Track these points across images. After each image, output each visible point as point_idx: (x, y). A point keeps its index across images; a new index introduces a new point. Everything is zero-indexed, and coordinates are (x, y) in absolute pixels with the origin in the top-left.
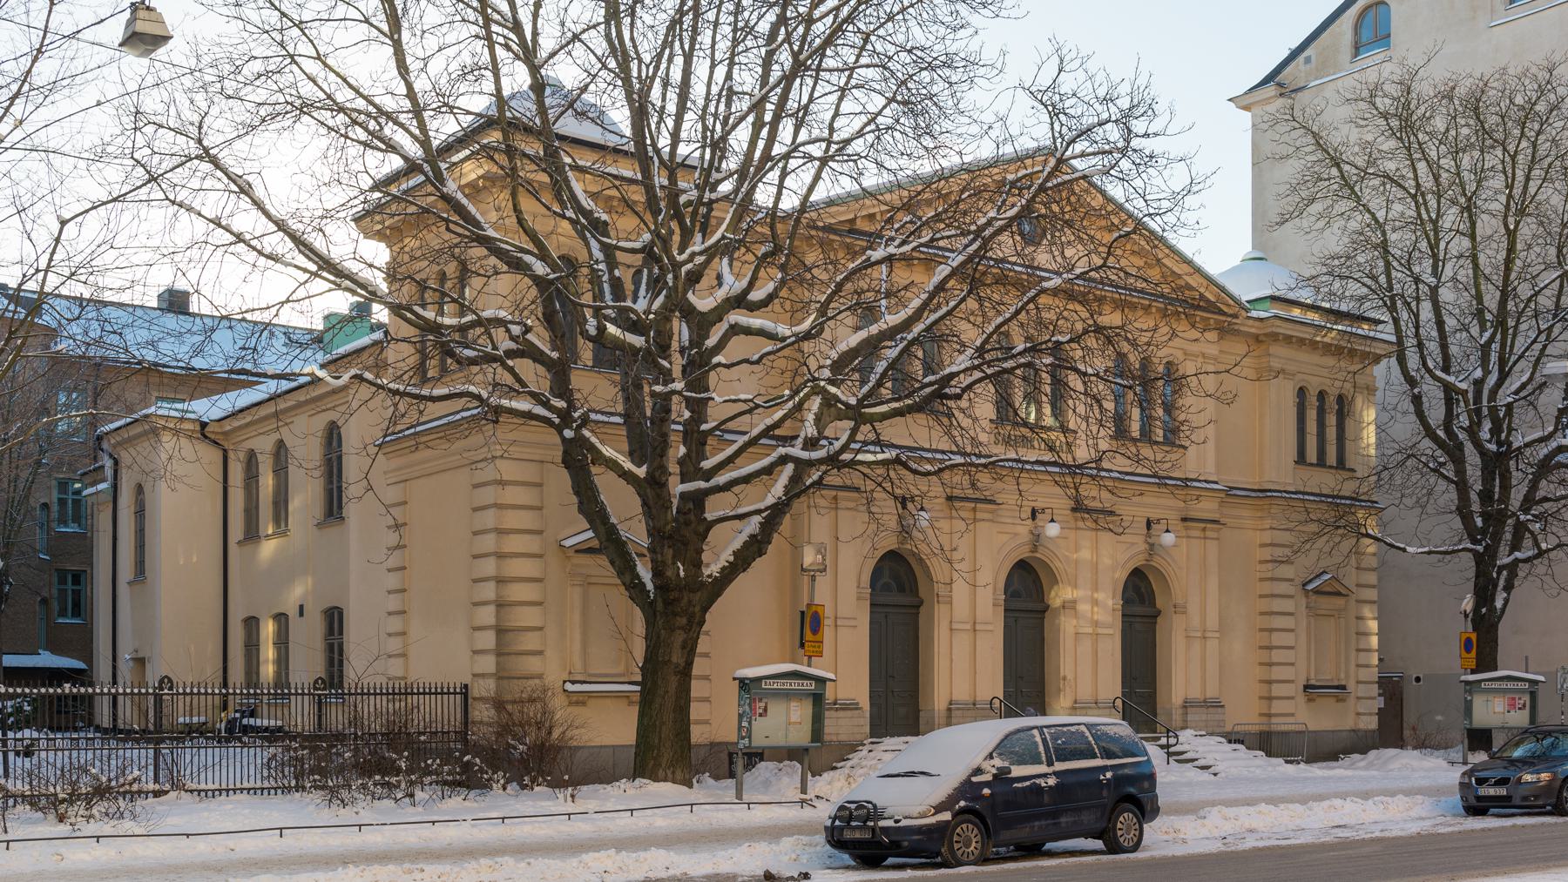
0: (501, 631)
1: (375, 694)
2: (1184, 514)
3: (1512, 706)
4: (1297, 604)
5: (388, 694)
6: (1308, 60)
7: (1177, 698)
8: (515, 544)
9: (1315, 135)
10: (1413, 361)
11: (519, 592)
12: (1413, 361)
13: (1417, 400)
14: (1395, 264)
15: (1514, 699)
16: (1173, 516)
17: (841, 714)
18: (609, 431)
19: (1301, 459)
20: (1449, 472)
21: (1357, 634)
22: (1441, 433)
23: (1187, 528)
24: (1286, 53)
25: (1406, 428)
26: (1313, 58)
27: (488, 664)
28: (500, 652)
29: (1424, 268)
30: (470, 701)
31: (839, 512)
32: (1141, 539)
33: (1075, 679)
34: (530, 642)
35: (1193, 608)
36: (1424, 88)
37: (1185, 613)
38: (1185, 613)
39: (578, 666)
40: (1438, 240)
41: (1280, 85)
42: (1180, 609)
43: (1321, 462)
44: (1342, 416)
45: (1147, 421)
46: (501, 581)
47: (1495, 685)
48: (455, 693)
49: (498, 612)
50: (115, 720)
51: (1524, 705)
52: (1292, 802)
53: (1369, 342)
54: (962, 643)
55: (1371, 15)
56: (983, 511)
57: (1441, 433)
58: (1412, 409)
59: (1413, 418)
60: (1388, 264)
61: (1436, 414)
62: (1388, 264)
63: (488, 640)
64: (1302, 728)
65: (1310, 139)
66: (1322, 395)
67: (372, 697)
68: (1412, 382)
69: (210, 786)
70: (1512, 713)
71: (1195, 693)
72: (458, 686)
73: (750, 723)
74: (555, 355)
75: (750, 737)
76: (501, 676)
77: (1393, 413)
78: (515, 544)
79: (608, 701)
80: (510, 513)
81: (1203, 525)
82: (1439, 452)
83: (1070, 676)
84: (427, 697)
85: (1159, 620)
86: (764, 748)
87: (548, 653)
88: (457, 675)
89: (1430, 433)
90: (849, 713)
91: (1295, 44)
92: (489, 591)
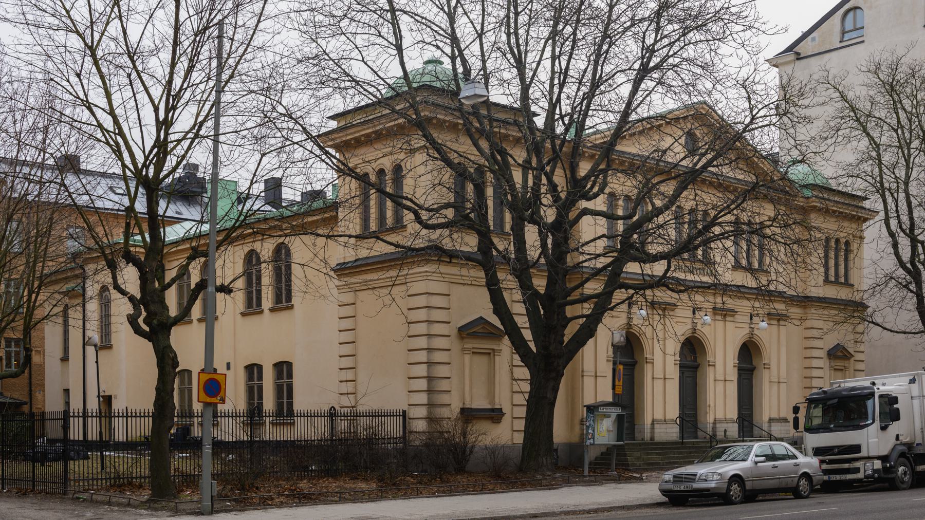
0: (430, 379)
1: (229, 416)
4: (824, 363)
5: (347, 416)
6: (814, 39)
7: (766, 418)
8: (437, 329)
9: (840, 93)
10: (894, 223)
11: (438, 357)
12: (894, 223)
13: (895, 245)
14: (886, 171)
16: (709, 306)
19: (827, 281)
20: (913, 287)
22: (909, 265)
24: (800, 34)
25: (889, 264)
26: (817, 39)
27: (423, 398)
28: (430, 391)
29: (901, 173)
30: (407, 419)
32: (747, 326)
33: (715, 406)
34: (443, 385)
35: (774, 366)
36: (904, 69)
37: (769, 368)
38: (714, 366)
40: (909, 155)
41: (798, 54)
42: (767, 367)
43: (836, 282)
44: (848, 251)
46: (430, 350)
48: (324, 416)
49: (428, 369)
50: (110, 436)
53: (870, 213)
54: (659, 385)
55: (851, 14)
57: (909, 265)
58: (892, 251)
59: (893, 257)
60: (881, 170)
61: (906, 254)
62: (881, 170)
63: (423, 384)
65: (838, 94)
66: (837, 241)
67: (309, 418)
68: (892, 234)
71: (774, 415)
72: (401, 411)
73: (594, 431)
74: (549, 234)
75: (594, 439)
76: (430, 405)
77: (882, 254)
78: (437, 329)
80: (434, 312)
82: (908, 277)
83: (712, 405)
84: (316, 418)
85: (755, 372)
87: (453, 392)
88: (400, 405)
89: (902, 264)
91: (806, 29)
92: (422, 356)
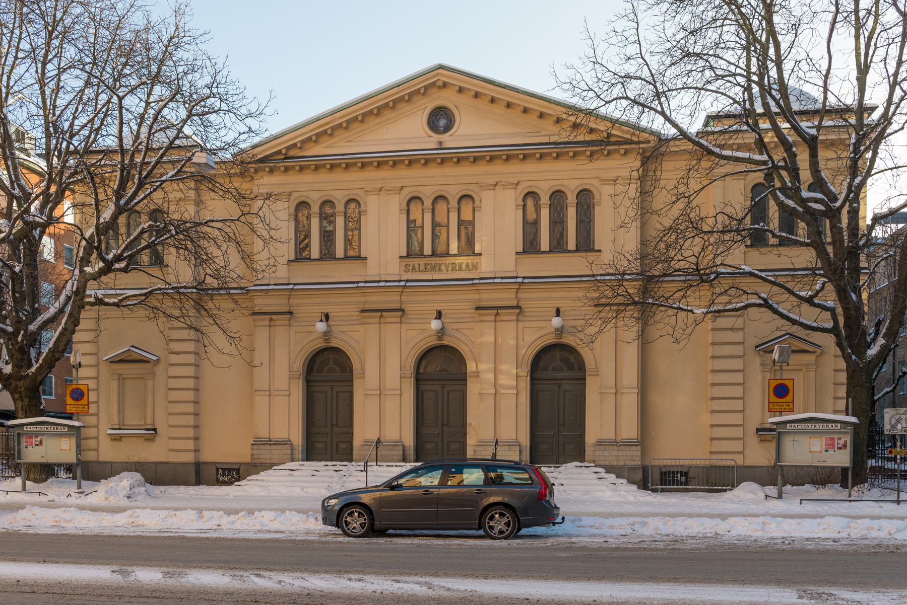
2: (477, 304)
3: (830, 445)
15: (833, 439)
17: (273, 447)
18: (365, 291)
21: (835, 384)
23: (480, 315)
31: (382, 325)
37: (597, 375)
39: (116, 421)
45: (327, 237)
47: (801, 426)
51: (845, 446)
52: (104, 511)
56: (389, 317)
64: (733, 463)
69: (6, 475)
70: (831, 452)
79: (134, 439)
81: (269, 317)
86: (241, 464)
90: (279, 447)
